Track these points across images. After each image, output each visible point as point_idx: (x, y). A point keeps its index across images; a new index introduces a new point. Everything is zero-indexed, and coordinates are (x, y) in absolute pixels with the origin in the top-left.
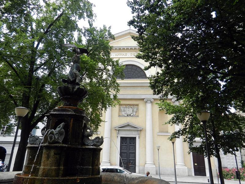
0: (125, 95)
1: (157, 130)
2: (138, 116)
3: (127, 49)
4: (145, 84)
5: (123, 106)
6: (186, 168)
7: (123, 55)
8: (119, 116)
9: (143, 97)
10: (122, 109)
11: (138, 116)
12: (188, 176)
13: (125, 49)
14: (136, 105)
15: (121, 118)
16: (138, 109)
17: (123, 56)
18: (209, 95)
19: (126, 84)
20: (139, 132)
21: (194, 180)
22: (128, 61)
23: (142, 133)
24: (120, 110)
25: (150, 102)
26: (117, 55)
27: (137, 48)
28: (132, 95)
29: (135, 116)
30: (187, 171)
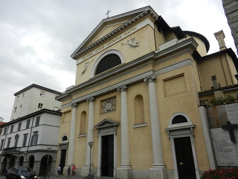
22: (105, 53)
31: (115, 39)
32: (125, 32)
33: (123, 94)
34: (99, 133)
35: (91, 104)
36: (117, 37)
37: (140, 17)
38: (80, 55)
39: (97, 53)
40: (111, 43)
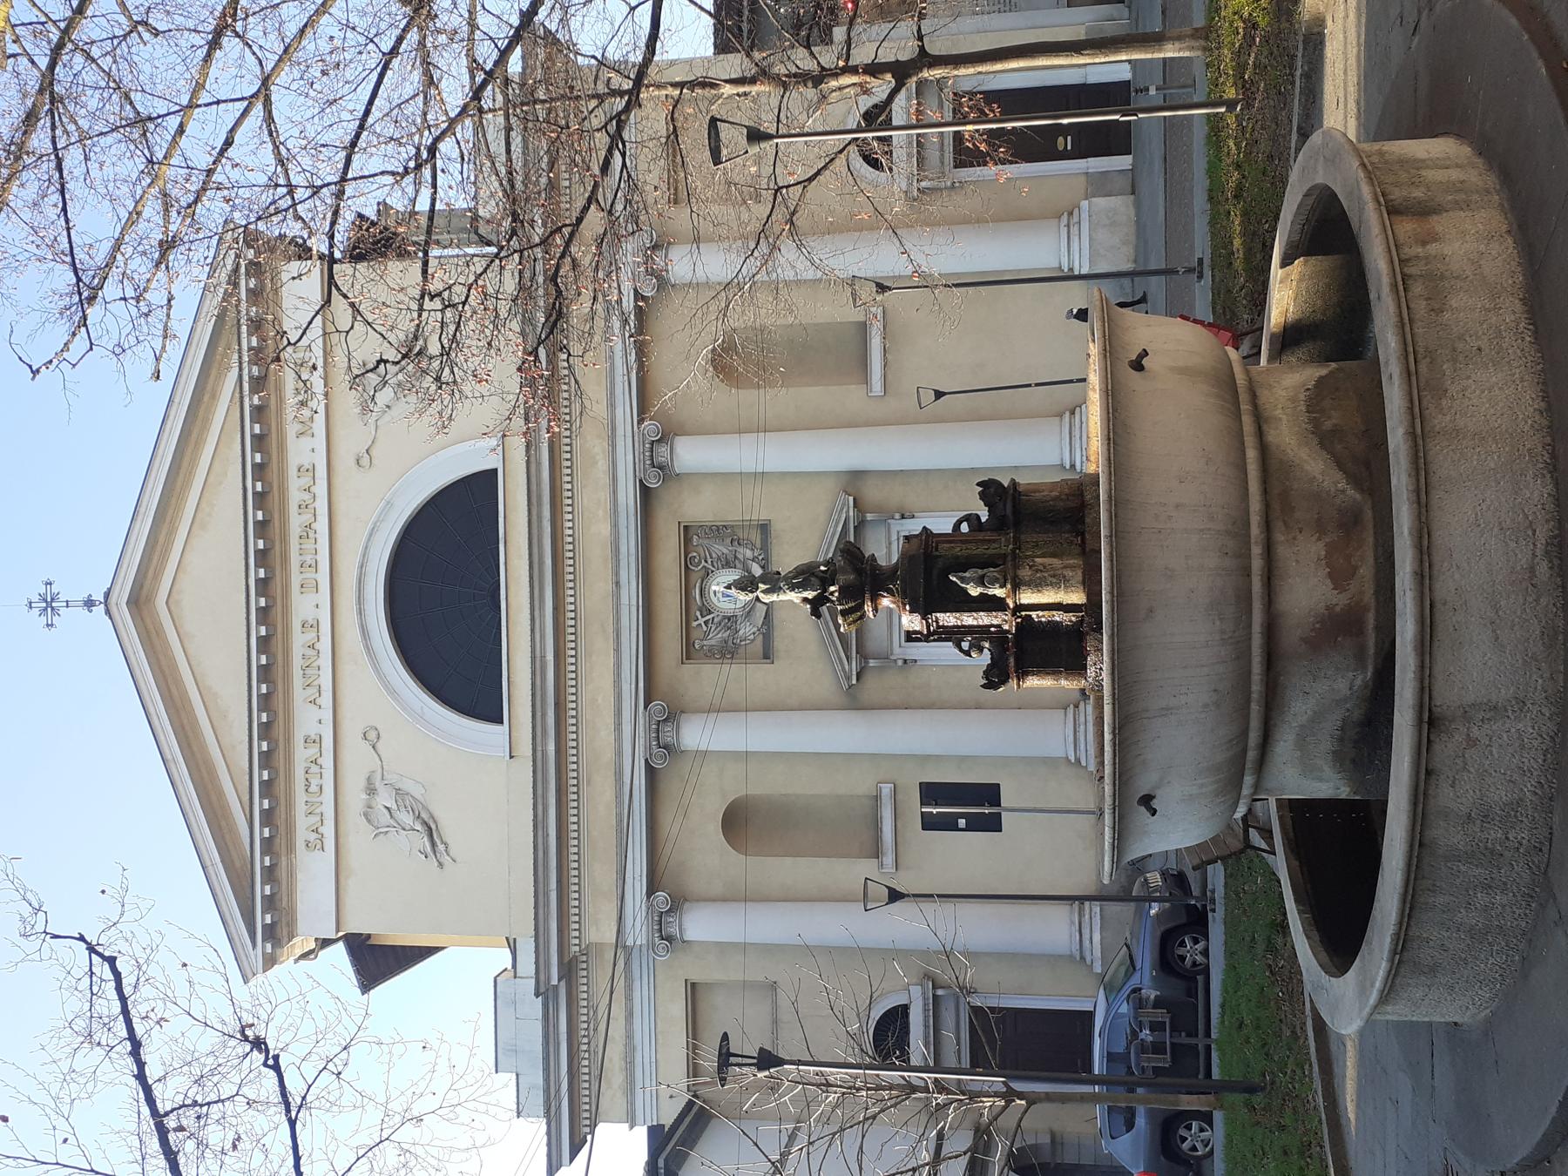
0: (618, 620)
1: (850, 397)
2: (765, 528)
3: (264, 615)
4: (539, 484)
5: (695, 634)
6: (1084, 204)
7: (312, 647)
8: (767, 655)
9: (628, 495)
10: (717, 637)
11: (765, 528)
12: (1133, 193)
13: (273, 924)
14: (687, 541)
15: (779, 643)
16: (719, 531)
17: (325, 645)
18: (735, 64)
19: (542, 616)
20: (869, 517)
21: (1297, 214)
23: (873, 493)
24: (728, 652)
25: (663, 450)
26: (312, 691)
27: (264, 660)
28: (617, 574)
29: (765, 547)
30: (1101, 202)
31: (296, 522)
32: (291, 429)
33: (690, 454)
34: (885, 657)
35: (694, 735)
36: (295, 496)
37: (270, 903)
38: (270, 874)
39: (326, 700)
40: (309, 559)
